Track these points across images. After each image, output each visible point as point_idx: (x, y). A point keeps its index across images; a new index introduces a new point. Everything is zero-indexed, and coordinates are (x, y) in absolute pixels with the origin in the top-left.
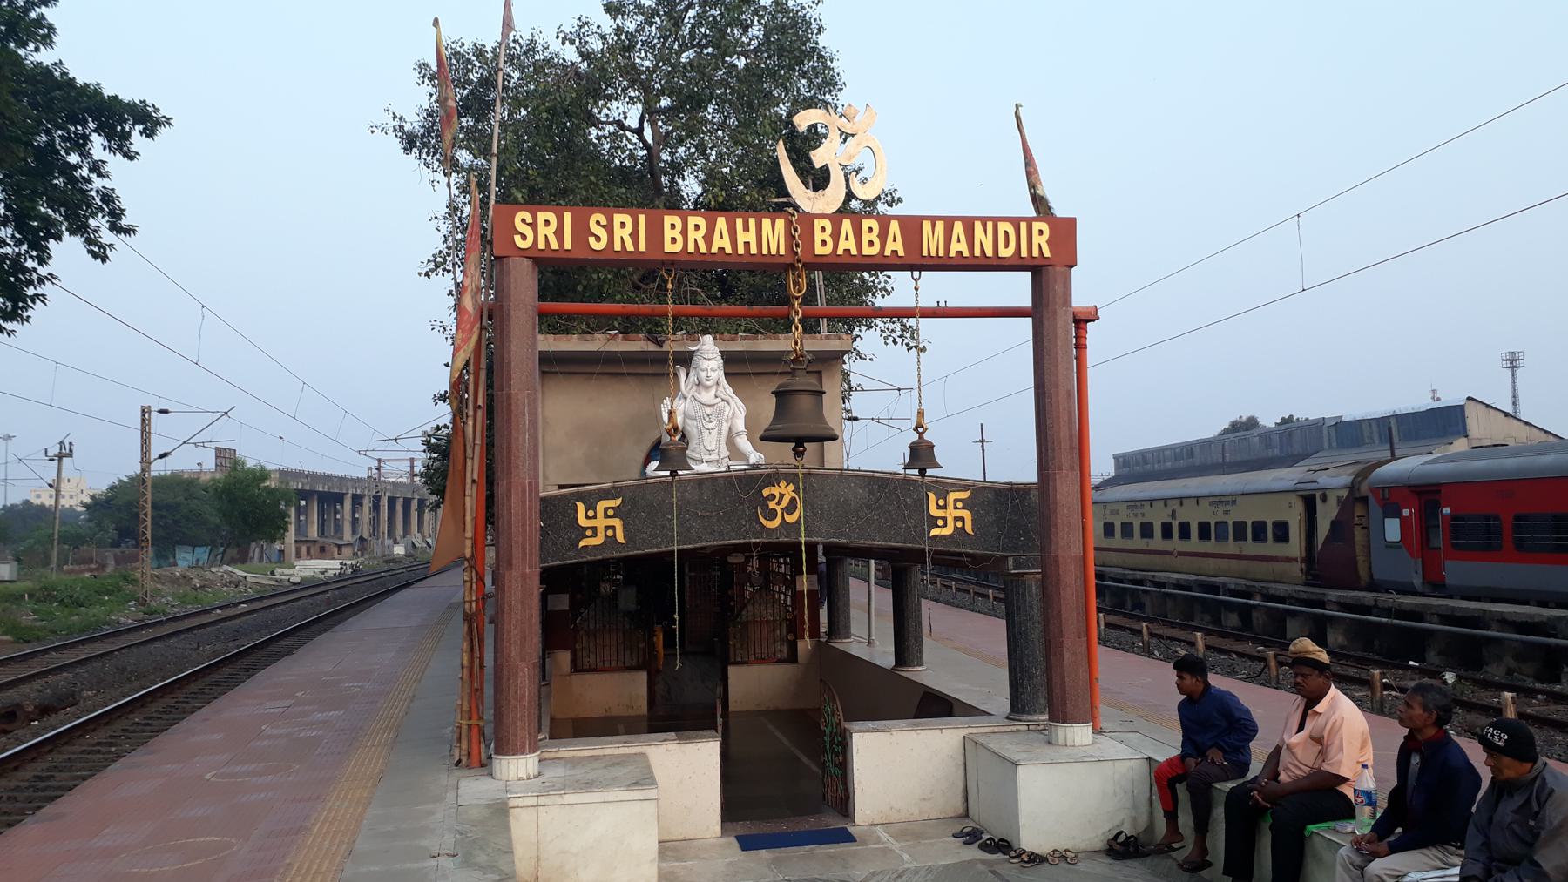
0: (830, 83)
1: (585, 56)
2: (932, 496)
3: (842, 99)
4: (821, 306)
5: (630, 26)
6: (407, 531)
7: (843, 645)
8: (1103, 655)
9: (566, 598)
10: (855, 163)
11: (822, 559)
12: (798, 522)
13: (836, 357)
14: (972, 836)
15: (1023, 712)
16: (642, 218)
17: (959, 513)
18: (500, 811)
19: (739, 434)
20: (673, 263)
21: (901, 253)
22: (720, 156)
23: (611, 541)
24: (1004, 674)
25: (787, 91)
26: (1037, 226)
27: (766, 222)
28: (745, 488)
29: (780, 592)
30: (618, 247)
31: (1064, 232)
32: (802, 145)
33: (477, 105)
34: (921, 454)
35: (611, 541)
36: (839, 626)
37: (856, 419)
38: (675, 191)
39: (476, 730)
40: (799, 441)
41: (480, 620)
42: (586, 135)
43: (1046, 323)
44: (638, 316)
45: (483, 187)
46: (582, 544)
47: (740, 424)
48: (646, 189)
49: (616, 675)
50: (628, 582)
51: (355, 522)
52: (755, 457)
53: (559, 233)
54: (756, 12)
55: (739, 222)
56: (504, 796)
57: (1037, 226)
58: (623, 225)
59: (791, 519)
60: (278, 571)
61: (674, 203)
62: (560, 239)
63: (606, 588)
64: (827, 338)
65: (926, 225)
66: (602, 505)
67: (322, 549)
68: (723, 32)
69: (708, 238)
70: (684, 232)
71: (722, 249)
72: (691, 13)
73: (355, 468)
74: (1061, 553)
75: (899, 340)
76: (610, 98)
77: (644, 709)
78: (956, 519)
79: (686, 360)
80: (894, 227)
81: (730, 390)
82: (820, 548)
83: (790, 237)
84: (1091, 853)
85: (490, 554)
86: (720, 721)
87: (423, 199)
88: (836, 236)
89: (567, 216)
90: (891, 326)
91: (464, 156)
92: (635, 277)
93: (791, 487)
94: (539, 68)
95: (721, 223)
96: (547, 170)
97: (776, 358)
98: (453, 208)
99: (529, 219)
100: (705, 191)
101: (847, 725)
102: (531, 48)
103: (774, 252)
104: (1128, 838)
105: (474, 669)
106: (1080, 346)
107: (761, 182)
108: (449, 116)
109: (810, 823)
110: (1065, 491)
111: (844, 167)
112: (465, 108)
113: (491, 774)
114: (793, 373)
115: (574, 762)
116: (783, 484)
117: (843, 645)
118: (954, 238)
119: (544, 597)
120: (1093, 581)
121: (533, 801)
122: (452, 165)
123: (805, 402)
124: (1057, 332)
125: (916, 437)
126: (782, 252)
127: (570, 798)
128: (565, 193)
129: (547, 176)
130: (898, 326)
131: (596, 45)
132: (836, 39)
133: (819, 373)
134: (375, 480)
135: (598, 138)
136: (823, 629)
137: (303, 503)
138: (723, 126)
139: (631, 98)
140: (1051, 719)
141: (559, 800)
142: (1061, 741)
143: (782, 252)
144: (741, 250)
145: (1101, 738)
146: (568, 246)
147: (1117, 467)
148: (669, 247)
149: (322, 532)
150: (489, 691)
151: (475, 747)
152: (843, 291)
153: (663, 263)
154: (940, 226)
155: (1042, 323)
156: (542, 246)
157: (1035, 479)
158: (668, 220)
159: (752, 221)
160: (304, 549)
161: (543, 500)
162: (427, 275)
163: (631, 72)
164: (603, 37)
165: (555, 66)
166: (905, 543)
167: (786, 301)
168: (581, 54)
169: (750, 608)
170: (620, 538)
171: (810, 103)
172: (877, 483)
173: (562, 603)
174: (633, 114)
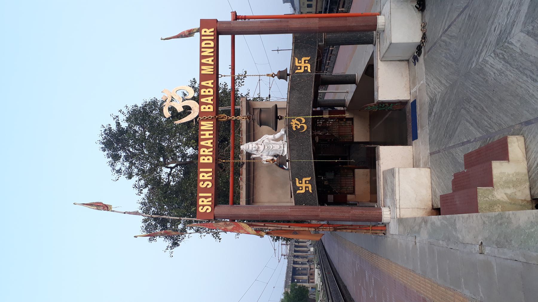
0: (154, 103)
1: (146, 186)
2: (297, 71)
3: (160, 98)
4: (230, 108)
5: (136, 170)
6: (306, 247)
7: (348, 102)
8: (353, 11)
9: (329, 196)
10: (181, 95)
11: (318, 109)
12: (305, 118)
13: (248, 102)
14: (416, 59)
15: (373, 40)
16: (201, 170)
17: (303, 62)
18: (401, 221)
19: (274, 137)
20: (216, 160)
21: (212, 81)
22: (180, 141)
23: (310, 182)
24: (359, 46)
25: (157, 118)
26: (203, 33)
27: (202, 128)
28: (293, 135)
29: (329, 123)
30: (211, 178)
31: (205, 24)
32: (175, 115)
33: (163, 222)
34: (282, 75)
35: (310, 182)
36: (342, 103)
37: (270, 95)
38: (192, 156)
39: (373, 228)
40: (277, 118)
41: (336, 227)
42: (173, 186)
43: (237, 30)
44: (234, 169)
45: (190, 222)
46: (311, 191)
47: (271, 137)
48: (191, 167)
49: (356, 179)
50: (324, 175)
51: (302, 264)
52: (282, 132)
53: (206, 198)
54: (131, 128)
55: (202, 137)
56: (396, 220)
57: (203, 33)
58: (203, 176)
59: (304, 121)
60: (318, 289)
61: (196, 157)
62: (208, 197)
63: (326, 183)
64: (241, 106)
65: (203, 72)
66: (298, 185)
67: (311, 274)
68: (137, 140)
69: (208, 148)
70: (206, 156)
71: (211, 143)
72: (131, 150)
73: (285, 263)
74: (317, 26)
75: (242, 80)
76: (160, 178)
77: (368, 170)
78: (305, 63)
79: (249, 155)
80: (203, 83)
81: (259, 140)
82: (314, 109)
83: (207, 120)
84: (423, 17)
85: (314, 222)
86: (373, 146)
87: (195, 241)
88: (207, 104)
89: (201, 195)
90: (238, 83)
91: (180, 226)
92: (221, 171)
93: (293, 120)
94: (150, 201)
95: (202, 143)
96: (185, 199)
97: (248, 125)
98: (197, 231)
99: (201, 207)
100: (191, 146)
101: (376, 102)
102: (144, 204)
103: (212, 125)
104: (418, 4)
105: (352, 228)
106: (245, 18)
107: (188, 127)
108: (167, 233)
109: (409, 116)
110: (295, 24)
111: (184, 100)
112: (164, 227)
113: (388, 223)
114: (254, 120)
115: (385, 195)
116: (292, 123)
117: (348, 102)
118: (207, 62)
119: (329, 204)
120: (327, 15)
121: (398, 210)
122: (183, 231)
123: (263, 116)
124: (240, 26)
125: (276, 77)
126: (212, 122)
127: (397, 197)
128: (192, 193)
129: (187, 200)
130: (238, 81)
131: (142, 182)
132: (139, 101)
133: (254, 109)
134: (288, 257)
135: (174, 182)
136: (342, 109)
137: (296, 281)
138: (169, 140)
139: (160, 171)
140: (375, 30)
141: (398, 201)
142: (383, 27)
143: (212, 122)
144: (212, 137)
145: (383, 13)
146: (210, 195)
147: (287, 2)
148: (211, 161)
149: (306, 275)
150: (360, 223)
151: (379, 228)
152: (225, 99)
153: (216, 163)
154: (203, 67)
155: (237, 32)
156: (210, 203)
157: (292, 34)
158: (201, 161)
159: (202, 133)
160: (311, 281)
161: (296, 204)
162: (220, 239)
163: (151, 170)
164: (140, 180)
165: (150, 196)
166: (312, 82)
167: (229, 121)
168: (146, 187)
169: (334, 134)
170: (309, 179)
171: (161, 110)
172: (292, 89)
173: (331, 198)
174: (166, 170)
